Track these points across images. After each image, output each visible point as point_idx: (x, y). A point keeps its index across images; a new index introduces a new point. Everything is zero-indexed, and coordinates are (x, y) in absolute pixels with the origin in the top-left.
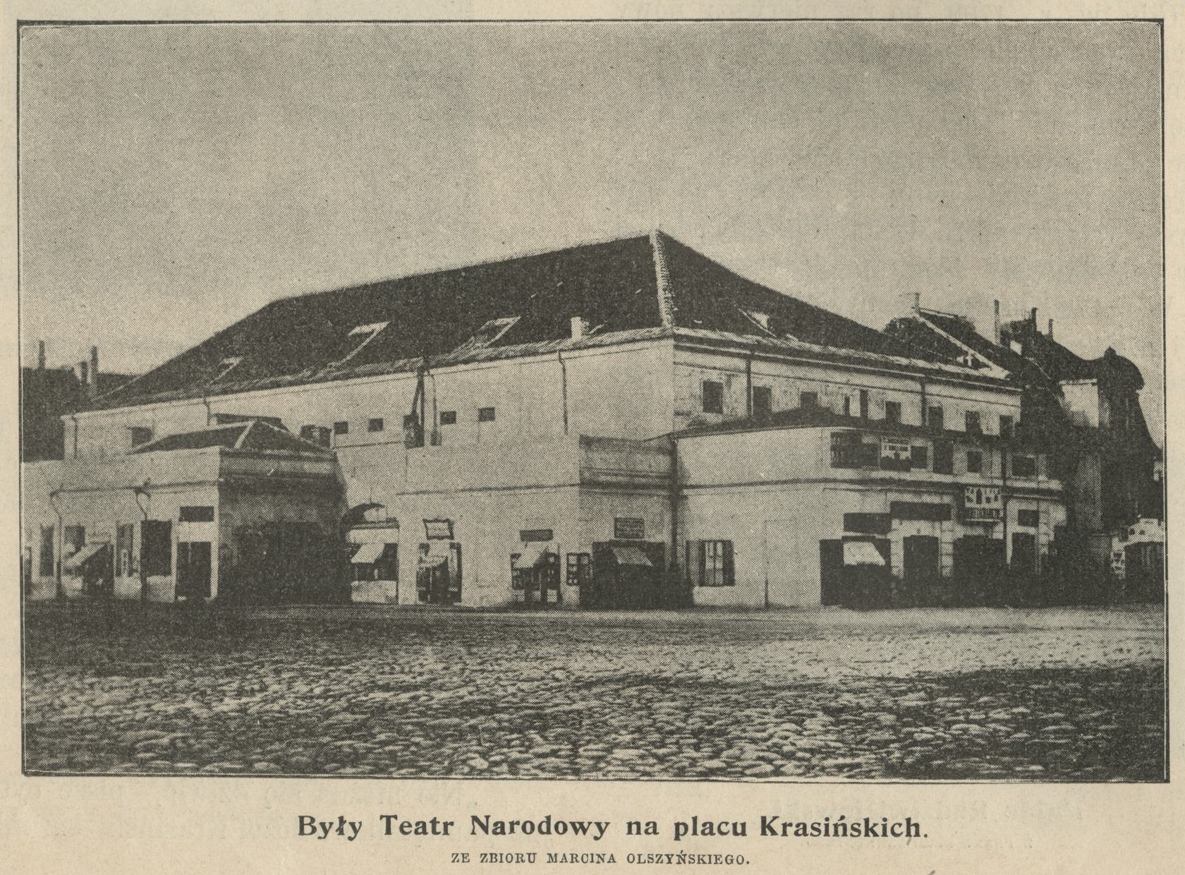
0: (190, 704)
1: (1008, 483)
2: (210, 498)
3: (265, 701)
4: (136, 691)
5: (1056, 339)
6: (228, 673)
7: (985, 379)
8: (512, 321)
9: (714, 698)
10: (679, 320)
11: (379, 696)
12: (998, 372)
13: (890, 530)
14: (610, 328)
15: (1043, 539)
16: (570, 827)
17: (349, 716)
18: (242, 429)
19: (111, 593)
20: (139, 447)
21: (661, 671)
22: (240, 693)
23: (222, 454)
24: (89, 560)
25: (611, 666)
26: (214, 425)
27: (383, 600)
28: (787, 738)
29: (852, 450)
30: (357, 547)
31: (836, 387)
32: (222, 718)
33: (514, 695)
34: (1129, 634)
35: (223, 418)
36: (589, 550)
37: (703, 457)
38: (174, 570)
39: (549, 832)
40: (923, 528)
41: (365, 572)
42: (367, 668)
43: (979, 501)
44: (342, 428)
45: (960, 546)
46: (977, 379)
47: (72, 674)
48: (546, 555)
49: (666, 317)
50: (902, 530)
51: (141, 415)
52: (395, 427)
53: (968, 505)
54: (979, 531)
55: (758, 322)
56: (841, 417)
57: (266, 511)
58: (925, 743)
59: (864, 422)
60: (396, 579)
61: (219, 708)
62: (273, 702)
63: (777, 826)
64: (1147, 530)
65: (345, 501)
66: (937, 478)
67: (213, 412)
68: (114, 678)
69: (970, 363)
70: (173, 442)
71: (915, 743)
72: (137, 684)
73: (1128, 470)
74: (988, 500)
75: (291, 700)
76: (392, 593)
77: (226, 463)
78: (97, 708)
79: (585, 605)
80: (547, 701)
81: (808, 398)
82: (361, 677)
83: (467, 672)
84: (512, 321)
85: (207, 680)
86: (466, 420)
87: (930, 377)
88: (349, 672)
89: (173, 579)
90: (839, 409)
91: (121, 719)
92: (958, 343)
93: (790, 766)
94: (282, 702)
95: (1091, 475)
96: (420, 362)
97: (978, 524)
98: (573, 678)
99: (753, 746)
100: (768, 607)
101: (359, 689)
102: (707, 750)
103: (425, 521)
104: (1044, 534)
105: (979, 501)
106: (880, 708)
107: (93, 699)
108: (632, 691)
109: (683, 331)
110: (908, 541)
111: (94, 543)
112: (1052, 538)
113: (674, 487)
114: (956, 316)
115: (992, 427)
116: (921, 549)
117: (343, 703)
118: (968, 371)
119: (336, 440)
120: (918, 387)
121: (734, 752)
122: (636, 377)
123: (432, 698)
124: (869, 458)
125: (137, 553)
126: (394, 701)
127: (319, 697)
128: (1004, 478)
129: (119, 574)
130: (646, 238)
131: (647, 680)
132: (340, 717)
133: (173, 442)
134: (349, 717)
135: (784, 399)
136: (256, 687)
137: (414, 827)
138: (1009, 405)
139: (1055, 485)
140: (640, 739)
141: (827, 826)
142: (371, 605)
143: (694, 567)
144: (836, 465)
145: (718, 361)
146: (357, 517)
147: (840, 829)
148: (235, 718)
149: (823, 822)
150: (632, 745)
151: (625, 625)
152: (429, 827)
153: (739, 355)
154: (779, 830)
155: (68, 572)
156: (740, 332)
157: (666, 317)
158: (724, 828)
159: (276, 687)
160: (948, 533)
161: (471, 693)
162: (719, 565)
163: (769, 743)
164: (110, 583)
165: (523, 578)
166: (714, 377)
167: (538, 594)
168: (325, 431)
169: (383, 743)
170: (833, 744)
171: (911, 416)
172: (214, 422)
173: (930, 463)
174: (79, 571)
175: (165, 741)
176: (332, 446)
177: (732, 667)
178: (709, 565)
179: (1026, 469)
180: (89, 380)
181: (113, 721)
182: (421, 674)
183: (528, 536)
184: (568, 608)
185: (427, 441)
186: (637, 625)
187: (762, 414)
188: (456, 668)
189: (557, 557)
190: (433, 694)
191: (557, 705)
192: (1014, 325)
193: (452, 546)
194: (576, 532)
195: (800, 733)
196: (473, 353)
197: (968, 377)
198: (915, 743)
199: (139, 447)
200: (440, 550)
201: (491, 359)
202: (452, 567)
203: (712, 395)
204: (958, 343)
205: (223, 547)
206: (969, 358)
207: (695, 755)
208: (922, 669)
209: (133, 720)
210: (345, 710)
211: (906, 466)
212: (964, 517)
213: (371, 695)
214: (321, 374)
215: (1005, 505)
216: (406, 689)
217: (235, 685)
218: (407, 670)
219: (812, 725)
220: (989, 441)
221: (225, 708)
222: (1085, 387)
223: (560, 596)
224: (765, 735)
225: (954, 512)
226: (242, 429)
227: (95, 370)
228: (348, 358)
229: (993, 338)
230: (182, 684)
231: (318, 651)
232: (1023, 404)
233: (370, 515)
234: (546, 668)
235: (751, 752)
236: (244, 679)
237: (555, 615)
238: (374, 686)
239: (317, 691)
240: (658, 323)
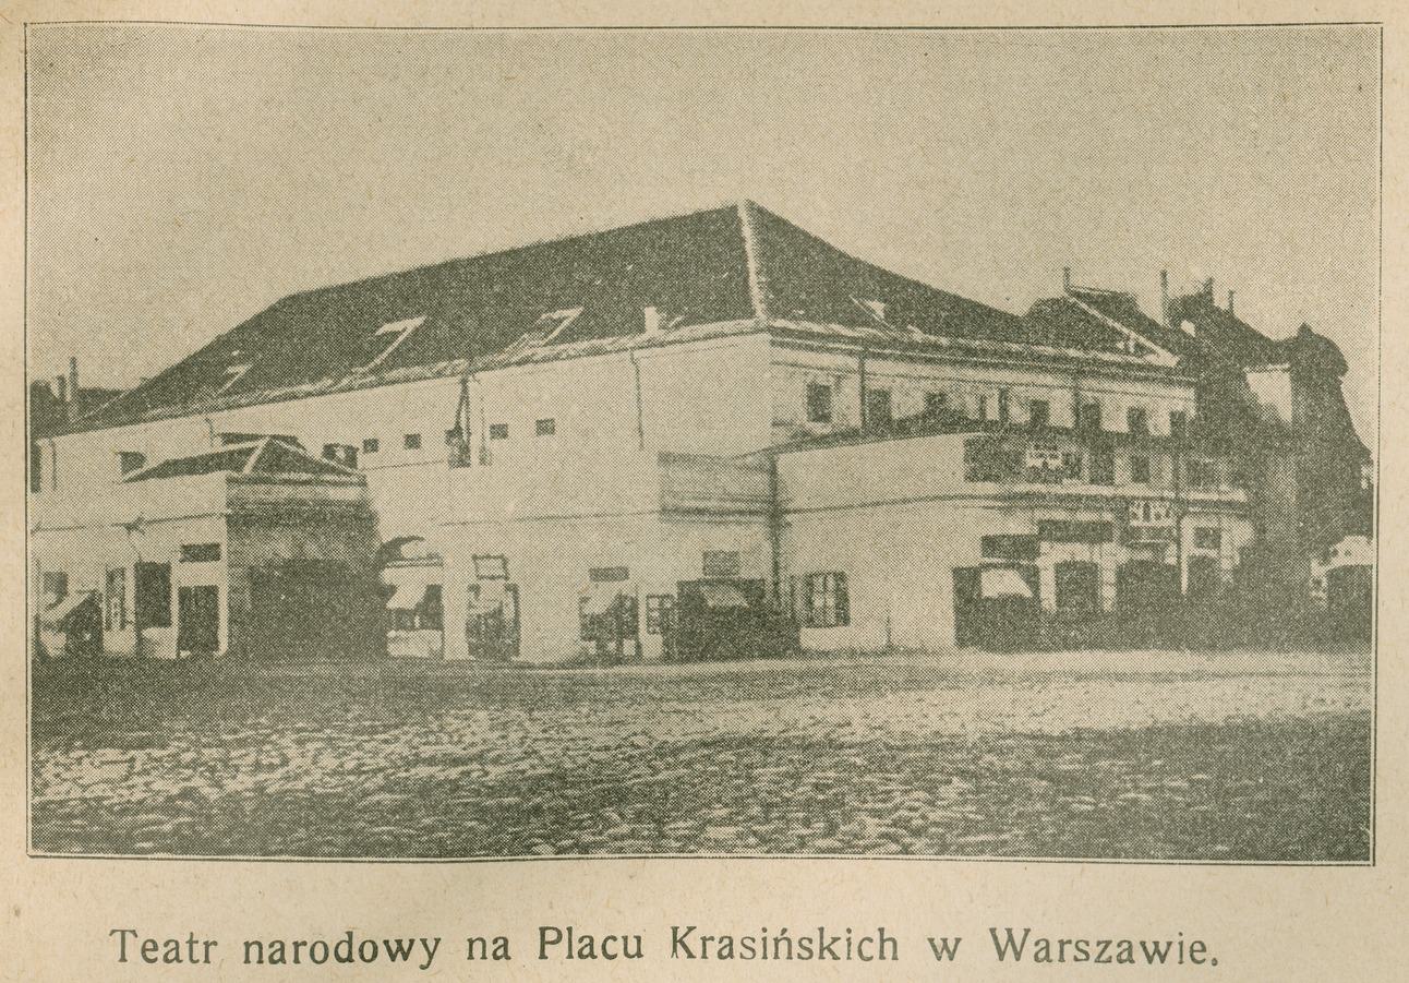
0: (197, 782)
1: (1182, 495)
2: (214, 531)
3: (287, 778)
4: (132, 767)
5: (1238, 314)
6: (242, 743)
7: (1151, 367)
8: (573, 313)
9: (826, 761)
10: (773, 311)
11: (423, 771)
12: (1165, 358)
13: (1039, 555)
14: (692, 319)
15: (1226, 565)
16: (382, 949)
17: (388, 796)
18: (250, 451)
19: (100, 648)
20: (132, 474)
21: (764, 731)
22: (258, 766)
23: (230, 481)
24: (75, 612)
25: (698, 727)
26: (220, 447)
27: (426, 655)
28: (916, 810)
29: (993, 452)
30: (393, 589)
31: (971, 387)
32: (235, 797)
33: (584, 767)
34: (1330, 680)
35: (229, 438)
36: (674, 592)
37: (806, 473)
38: (175, 619)
39: (350, 959)
40: (1081, 552)
41: (402, 618)
42: (409, 737)
43: (1147, 516)
44: (372, 445)
45: (1122, 574)
46: (1141, 368)
47: (55, 748)
48: (621, 598)
49: (759, 308)
50: (1051, 556)
51: (132, 437)
52: (436, 447)
53: (1134, 523)
54: (1146, 555)
55: (873, 311)
56: (976, 422)
57: (280, 546)
58: (1087, 816)
59: (1004, 425)
60: (440, 627)
61: (231, 786)
62: (295, 779)
63: (694, 943)
64: (1350, 551)
65: (373, 535)
66: (1094, 490)
67: (216, 432)
68: (108, 750)
69: (1132, 350)
70: (169, 469)
71: (1072, 816)
72: (132, 760)
73: (1342, 487)
74: (1158, 517)
75: (318, 776)
76: (437, 646)
77: (234, 491)
78: (85, 788)
79: (667, 659)
80: (625, 771)
81: (935, 401)
82: (400, 748)
83: (528, 741)
84: (573, 313)
85: (215, 752)
86: (521, 431)
87: (1080, 371)
88: (386, 741)
89: (174, 631)
90: (973, 416)
91: (116, 800)
92: (1117, 326)
93: (919, 843)
94: (307, 779)
95: (1284, 482)
96: (462, 363)
97: (1146, 546)
98: (655, 744)
99: (877, 820)
100: (890, 649)
101: (399, 763)
102: (820, 825)
103: (475, 558)
104: (1227, 559)
105: (1147, 516)
106: (1028, 771)
107: (95, 774)
108: (728, 756)
109: (780, 323)
110: (1061, 568)
111: (80, 592)
112: (1237, 562)
113: (775, 514)
114: (1115, 293)
115: (1160, 425)
116: (1078, 579)
117: (380, 779)
118: (1131, 359)
119: (363, 459)
120: (1070, 383)
121: (854, 827)
122: (724, 382)
123: (487, 774)
124: (1012, 465)
125: (130, 603)
126: (441, 777)
127: (351, 773)
128: (1176, 487)
129: (109, 628)
130: (734, 209)
131: (748, 742)
132: (376, 798)
133: (169, 469)
134: (386, 797)
135: (908, 402)
136: (276, 761)
137: (162, 950)
138: (1182, 399)
139: (1240, 496)
140: (737, 814)
141: (764, 939)
142: (409, 661)
143: (800, 604)
144: (972, 477)
145: (826, 359)
146: (391, 552)
147: (783, 945)
148: (250, 799)
149: (759, 936)
150: (728, 821)
151: (718, 677)
152: (184, 952)
153: (851, 353)
154: (696, 948)
155: (49, 626)
156: (851, 323)
157: (759, 308)
158: (612, 947)
159: (299, 761)
160: (1109, 557)
161: (533, 767)
162: (831, 602)
163: (895, 816)
164: (98, 639)
165: (592, 627)
166: (822, 380)
167: (612, 646)
168: (351, 453)
169: (430, 830)
170: (972, 816)
171: (1061, 414)
172: (218, 441)
173: (1086, 473)
174: (62, 626)
175: (167, 828)
176: (360, 466)
177: (849, 724)
178: (818, 603)
179: (1200, 476)
180: (68, 398)
181: (105, 803)
182: (473, 744)
183: (599, 575)
184: (651, 662)
185: (474, 458)
186: (737, 678)
187: (881, 422)
188: (514, 737)
189: (635, 603)
190: (489, 768)
191: (639, 776)
192: (1185, 301)
193: (508, 588)
194: (663, 565)
195: (931, 803)
196: (529, 353)
197: (1129, 365)
198: (1072, 816)
199: (132, 474)
200: (493, 593)
201: (545, 360)
202: (508, 614)
203: (818, 399)
204: (1117, 326)
205: (233, 590)
206: (1131, 344)
207: (805, 832)
208: (1080, 725)
209: (129, 802)
210: (382, 789)
211: (1057, 476)
212: (1129, 537)
213: (413, 771)
214: (345, 381)
215: (1178, 522)
216: (456, 762)
217: (251, 759)
218: (456, 739)
219: (949, 792)
220: (1163, 445)
221: (240, 788)
222: (1275, 374)
223: (639, 646)
224: (889, 805)
225: (1117, 533)
226: (250, 451)
227: (75, 385)
228: (377, 361)
229: (1161, 320)
230: (188, 757)
231: (350, 716)
232: (1199, 398)
233: (406, 550)
234: (624, 735)
235: (873, 827)
236: (260, 752)
237: (634, 670)
238: (418, 760)
239: (350, 765)
240: (751, 314)
